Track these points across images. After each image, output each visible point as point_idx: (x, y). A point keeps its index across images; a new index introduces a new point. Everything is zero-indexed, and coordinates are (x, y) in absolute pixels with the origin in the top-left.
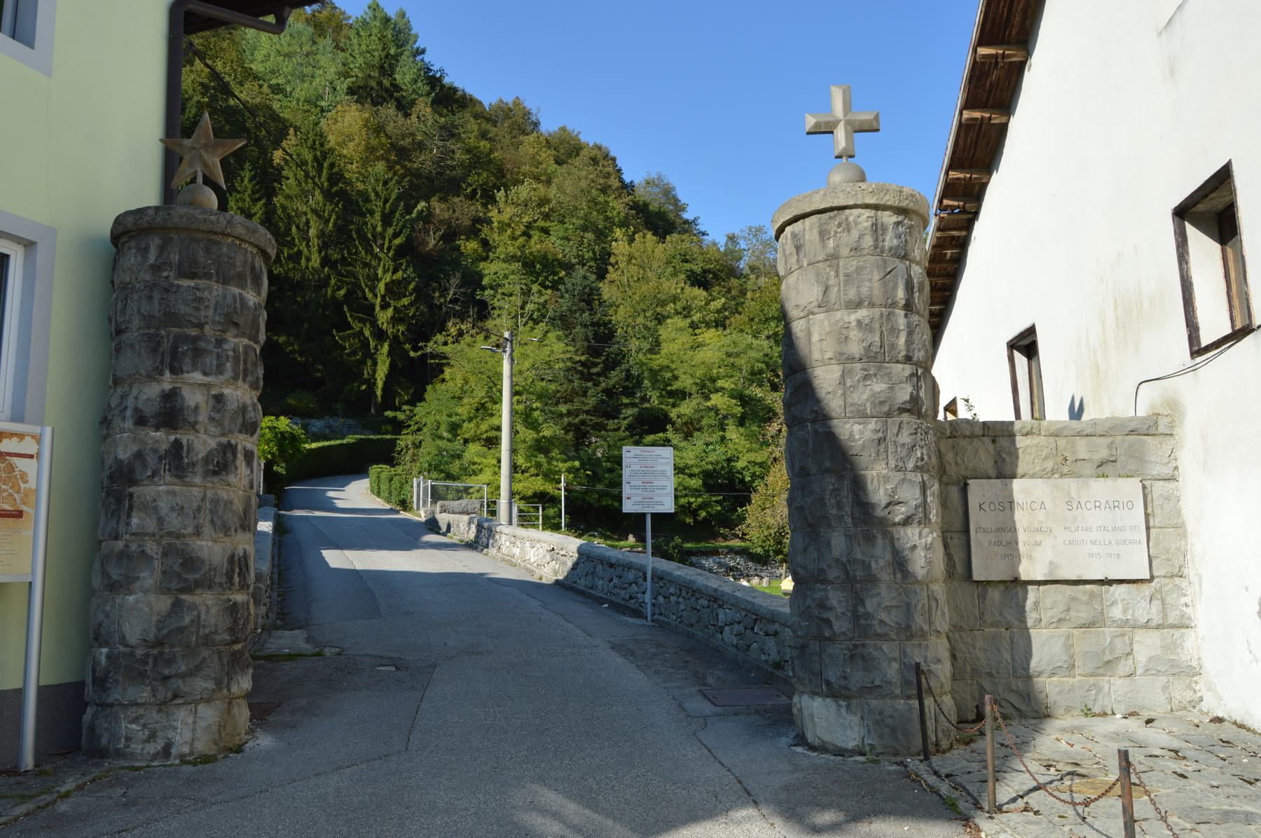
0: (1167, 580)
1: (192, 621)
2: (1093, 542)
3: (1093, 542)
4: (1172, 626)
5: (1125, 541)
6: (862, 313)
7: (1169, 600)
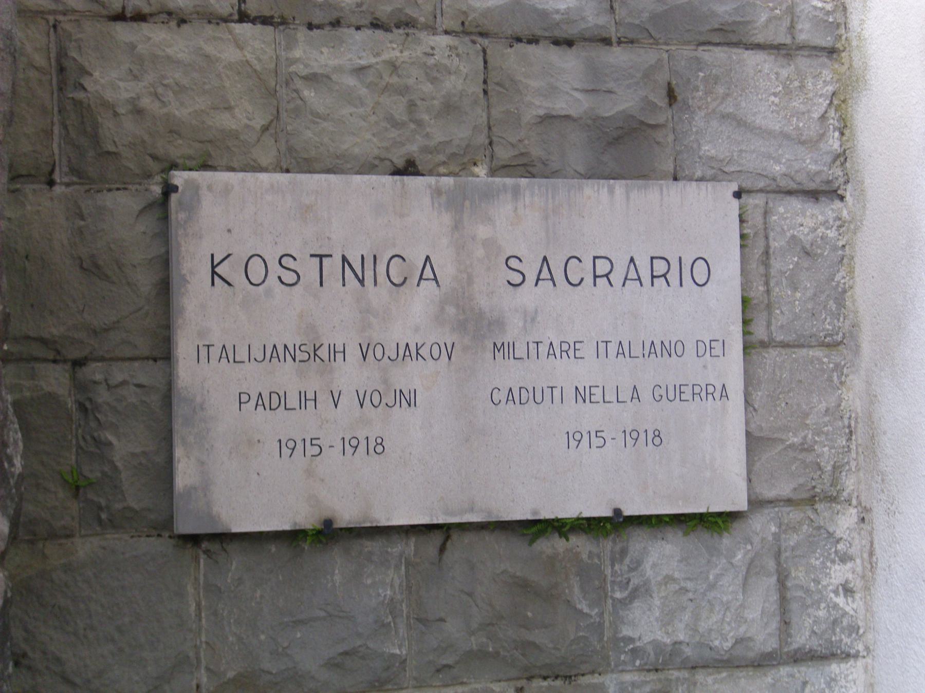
0: (793, 515)
1: (77, 454)
2: (582, 395)
3: (582, 395)
4: (801, 657)
5: (679, 390)
6: (78, 621)
7: (798, 575)
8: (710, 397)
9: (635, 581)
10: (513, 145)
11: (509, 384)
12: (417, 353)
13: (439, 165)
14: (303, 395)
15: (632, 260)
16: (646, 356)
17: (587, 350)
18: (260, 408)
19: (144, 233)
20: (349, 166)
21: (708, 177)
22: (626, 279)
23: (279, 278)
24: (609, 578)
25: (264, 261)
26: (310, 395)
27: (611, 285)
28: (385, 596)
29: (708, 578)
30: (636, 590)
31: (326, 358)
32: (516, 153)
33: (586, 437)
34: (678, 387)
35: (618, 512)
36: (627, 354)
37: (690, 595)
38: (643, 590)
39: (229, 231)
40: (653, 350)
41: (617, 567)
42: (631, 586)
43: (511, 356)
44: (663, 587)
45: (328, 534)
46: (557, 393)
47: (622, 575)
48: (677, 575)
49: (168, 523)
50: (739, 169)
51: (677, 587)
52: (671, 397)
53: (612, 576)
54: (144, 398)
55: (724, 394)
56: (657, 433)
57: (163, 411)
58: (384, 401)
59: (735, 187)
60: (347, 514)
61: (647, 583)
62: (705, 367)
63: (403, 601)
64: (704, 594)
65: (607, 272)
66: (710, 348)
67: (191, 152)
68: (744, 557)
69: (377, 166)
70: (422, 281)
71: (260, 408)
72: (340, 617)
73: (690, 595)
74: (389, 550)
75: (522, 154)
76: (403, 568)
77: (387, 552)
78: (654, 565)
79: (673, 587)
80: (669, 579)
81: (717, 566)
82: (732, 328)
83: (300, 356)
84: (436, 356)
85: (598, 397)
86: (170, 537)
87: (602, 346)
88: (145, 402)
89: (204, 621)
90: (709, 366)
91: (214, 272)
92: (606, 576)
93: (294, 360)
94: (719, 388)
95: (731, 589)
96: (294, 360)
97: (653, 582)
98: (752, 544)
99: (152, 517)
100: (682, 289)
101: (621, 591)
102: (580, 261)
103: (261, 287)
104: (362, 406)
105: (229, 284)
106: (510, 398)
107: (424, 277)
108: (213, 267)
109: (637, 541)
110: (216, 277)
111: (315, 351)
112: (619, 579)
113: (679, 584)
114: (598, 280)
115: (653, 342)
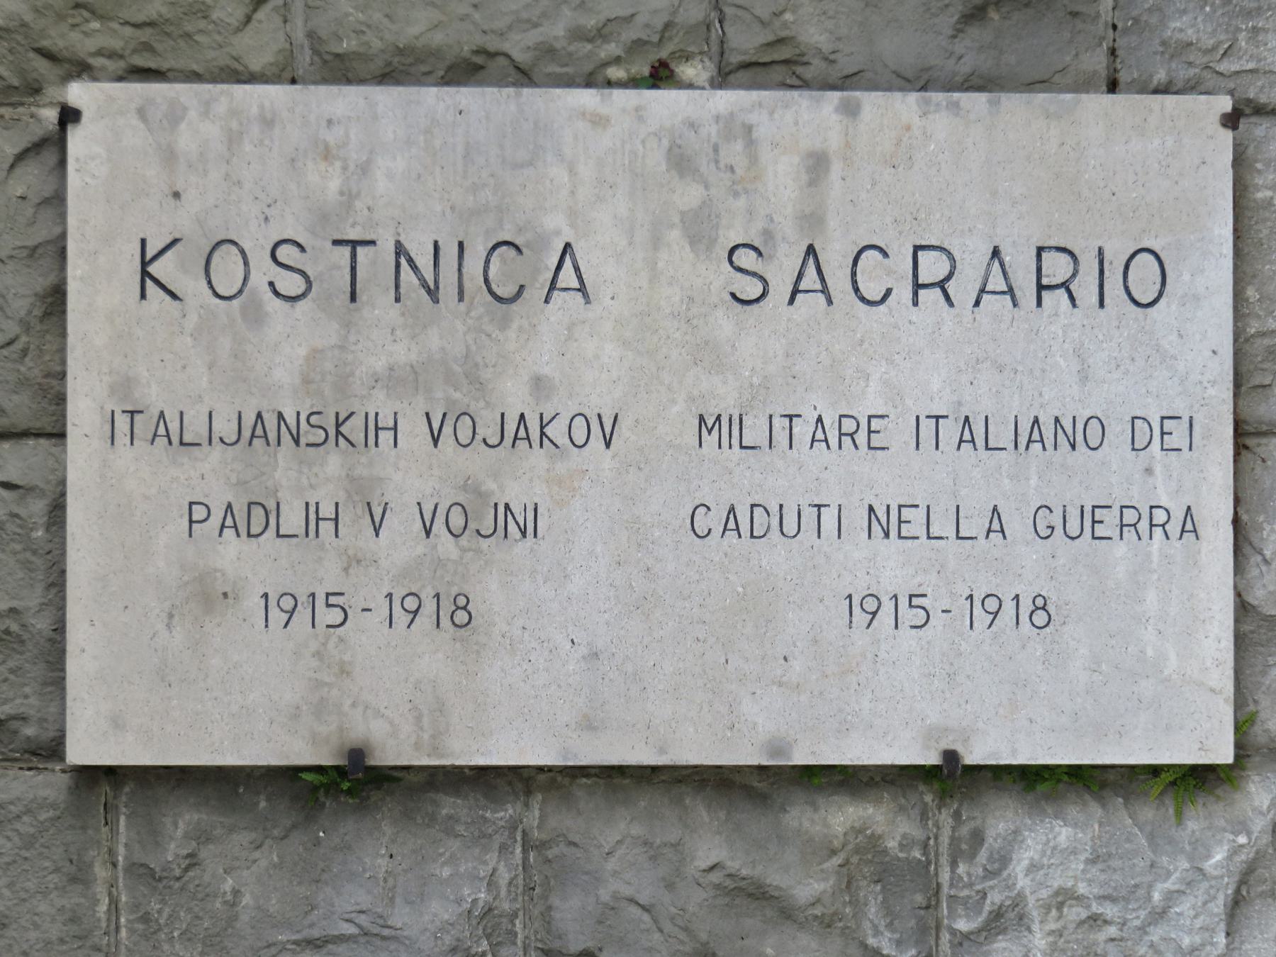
2: (884, 522)
3: (884, 522)
5: (1092, 516)
8: (1158, 532)
9: (995, 898)
10: (763, 23)
11: (728, 498)
12: (543, 434)
13: (606, 64)
14: (312, 509)
15: (996, 253)
16: (1022, 446)
17: (897, 434)
18: (229, 533)
19: (23, 198)
20: (424, 68)
21: (1180, 85)
22: (982, 290)
23: (271, 284)
24: (945, 889)
25: (857, 290)
26: (327, 511)
27: (951, 304)
28: (475, 901)
29: (1149, 898)
30: (998, 914)
31: (358, 437)
32: (771, 38)
33: (888, 606)
34: (1088, 509)
35: (951, 756)
36: (980, 442)
37: (1112, 931)
38: (1012, 915)
39: (177, 195)
40: (1036, 436)
41: (962, 869)
42: (987, 908)
43: (735, 441)
44: (1054, 912)
45: (353, 784)
46: (829, 517)
47: (971, 885)
48: (1082, 889)
49: (54, 749)
50: (1251, 66)
51: (1084, 915)
52: (1073, 528)
53: (951, 886)
54: (16, 510)
55: (1189, 526)
56: (1040, 602)
57: (1088, 92)
58: (472, 526)
59: (1225, 104)
60: (396, 748)
61: (1018, 901)
62: (1149, 471)
63: (515, 915)
64: (1143, 929)
65: (942, 277)
66: (1158, 433)
67: (116, 44)
68: (1230, 858)
69: (482, 67)
70: (556, 293)
71: (229, 533)
72: (384, 938)
73: (1112, 931)
74: (488, 815)
75: (781, 41)
76: (518, 850)
77: (485, 820)
78: (1033, 867)
79: (1075, 913)
80: (1064, 898)
81: (1169, 874)
82: (1211, 391)
83: (309, 435)
84: (580, 440)
85: (917, 528)
86: (63, 771)
87: (927, 427)
88: (17, 516)
89: (123, 933)
90: (1158, 469)
91: (145, 274)
92: (939, 885)
93: (297, 442)
94: (1178, 515)
95: (1199, 923)
96: (297, 442)
97: (1031, 901)
98: (1249, 834)
99: (29, 731)
100: (1102, 313)
101: (967, 916)
102: (886, 255)
103: (235, 302)
104: (428, 533)
105: (173, 295)
106: (731, 525)
107: (560, 284)
108: (144, 264)
109: (1001, 819)
110: (149, 283)
111: (338, 425)
112: (966, 892)
113: (1088, 907)
114: (921, 292)
115: (1036, 421)
